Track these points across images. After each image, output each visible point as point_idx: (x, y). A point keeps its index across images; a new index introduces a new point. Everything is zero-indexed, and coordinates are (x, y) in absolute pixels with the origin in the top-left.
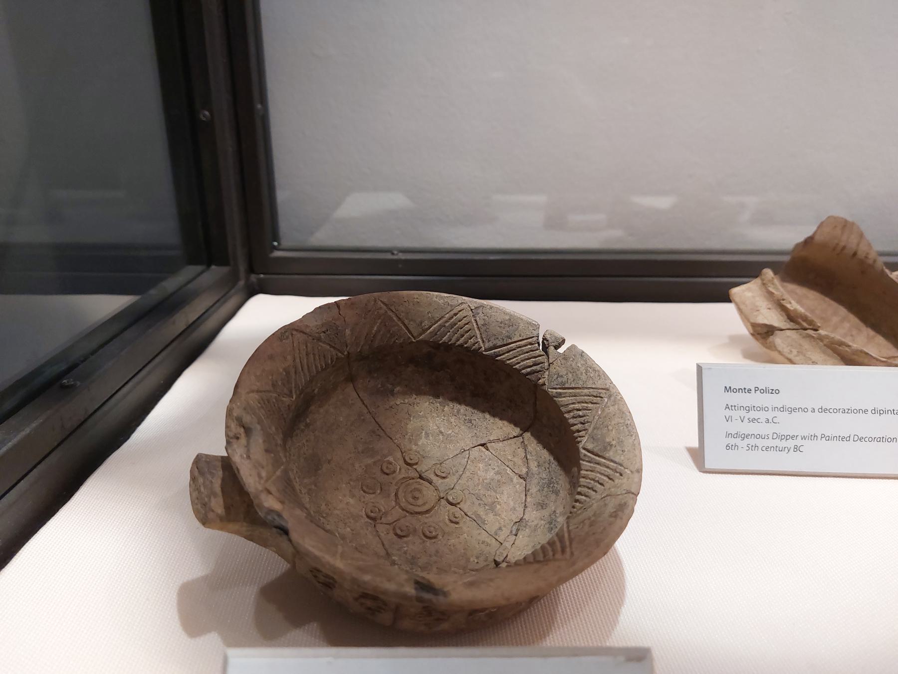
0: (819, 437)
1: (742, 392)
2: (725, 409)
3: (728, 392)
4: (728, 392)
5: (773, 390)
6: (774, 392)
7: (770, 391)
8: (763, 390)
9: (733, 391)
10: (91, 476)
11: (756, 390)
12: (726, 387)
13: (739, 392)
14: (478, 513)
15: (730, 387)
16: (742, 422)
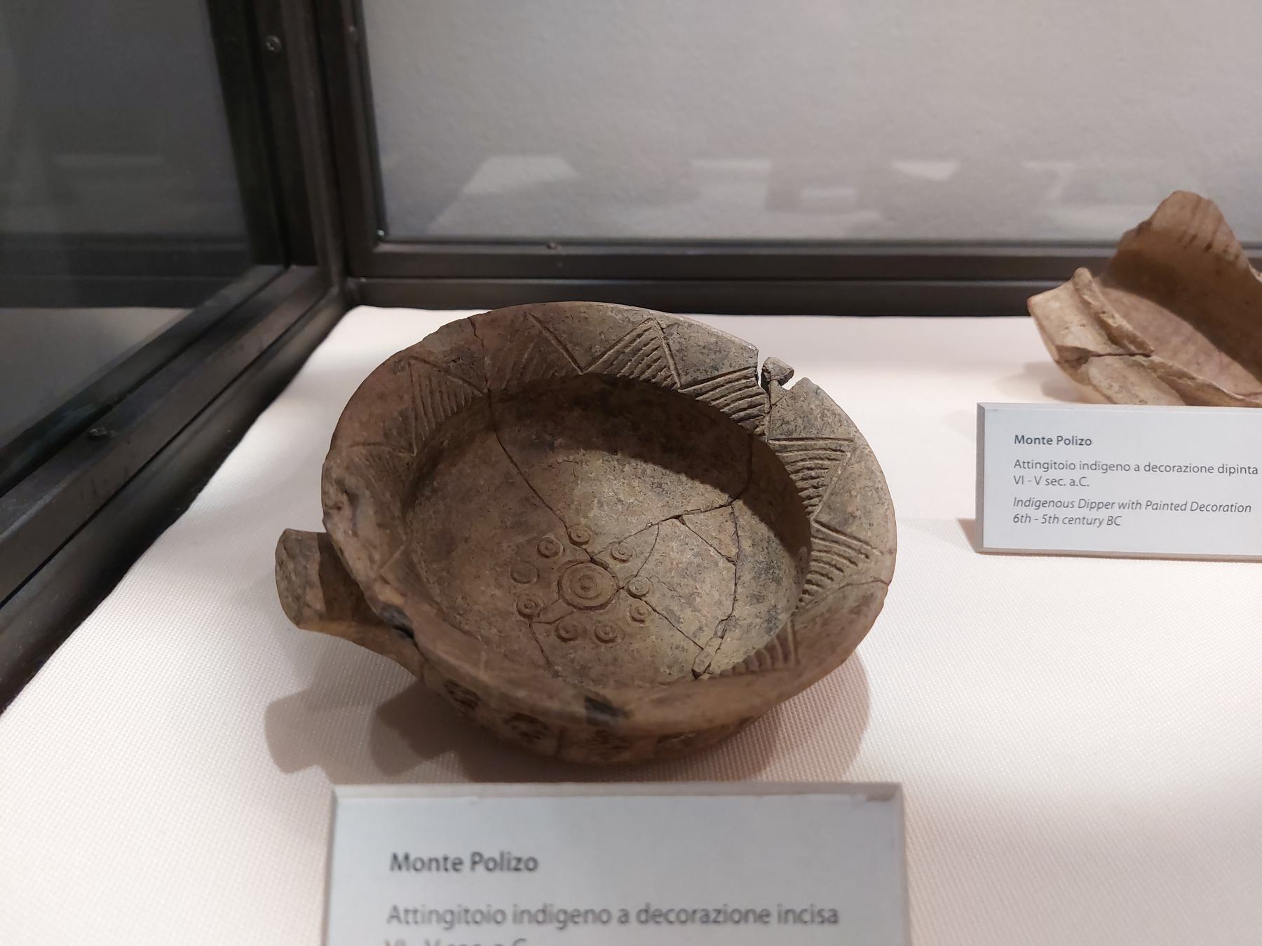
1: (1039, 443)
3: (1020, 442)
4: (1020, 442)
7: (1079, 442)
11: (474, 863)
12: (1017, 436)
15: (1023, 437)
16: (1038, 484)
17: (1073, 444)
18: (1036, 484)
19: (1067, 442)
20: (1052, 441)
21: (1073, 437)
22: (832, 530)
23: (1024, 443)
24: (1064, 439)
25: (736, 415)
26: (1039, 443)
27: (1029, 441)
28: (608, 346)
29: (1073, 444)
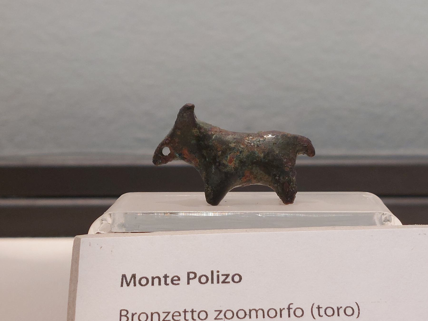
0: (184, 279)
1: (160, 284)
2: (188, 283)
3: (128, 285)
4: (128, 285)
5: (227, 276)
6: (229, 279)
7: (222, 278)
8: (207, 277)
9: (233, 280)
10: (416, 225)
11: (189, 279)
12: (124, 276)
13: (153, 284)
14: (302, 139)
15: (134, 276)
16: (216, 319)
17: (212, 282)
18: (215, 317)
19: (204, 279)
20: (179, 279)
21: (212, 272)
22: (283, 212)
23: (135, 285)
24: (197, 279)
25: (298, 215)
26: (160, 284)
27: (144, 282)
28: (214, 213)
29: (212, 282)
